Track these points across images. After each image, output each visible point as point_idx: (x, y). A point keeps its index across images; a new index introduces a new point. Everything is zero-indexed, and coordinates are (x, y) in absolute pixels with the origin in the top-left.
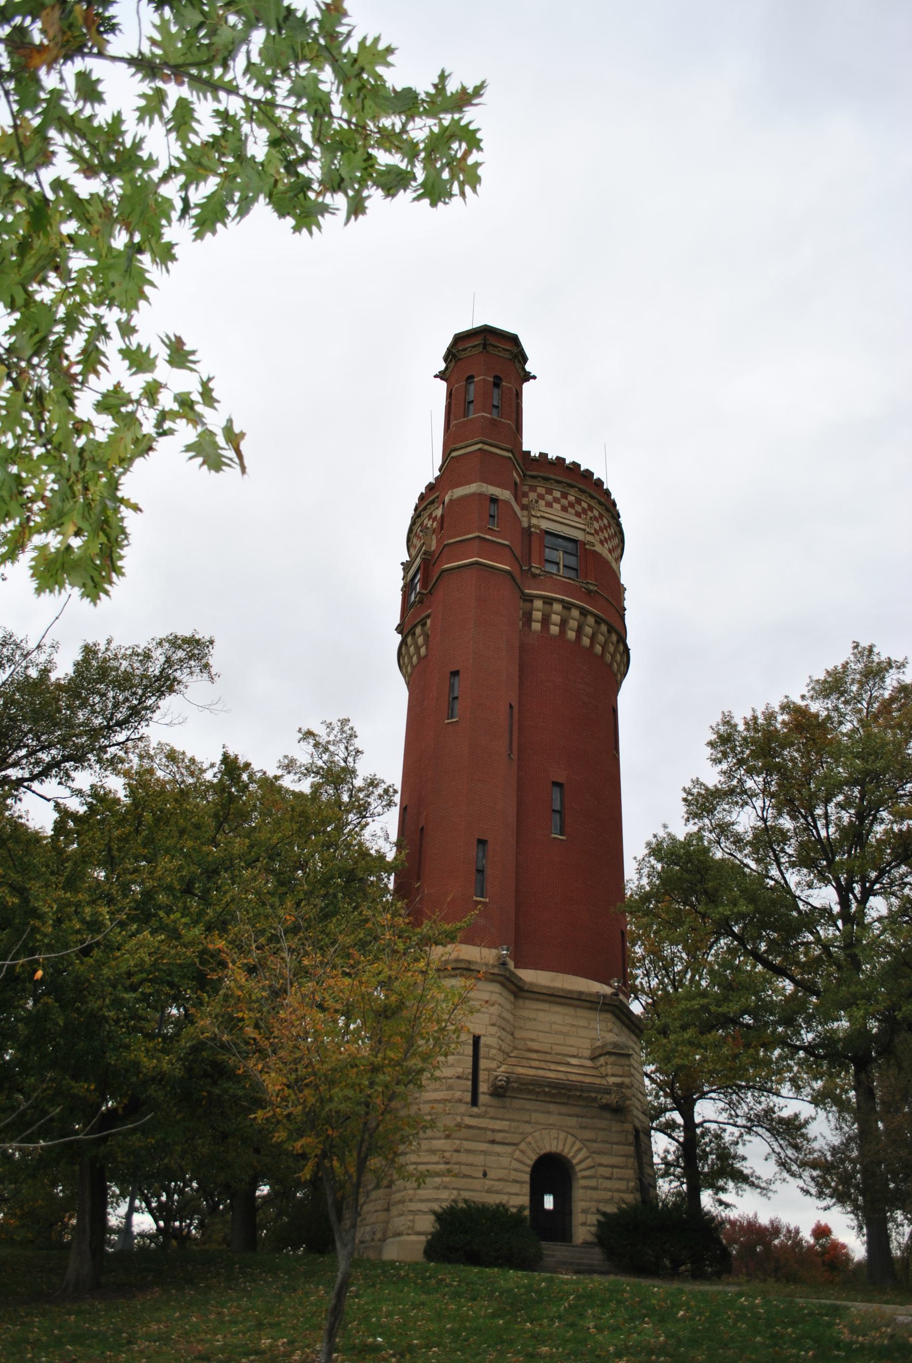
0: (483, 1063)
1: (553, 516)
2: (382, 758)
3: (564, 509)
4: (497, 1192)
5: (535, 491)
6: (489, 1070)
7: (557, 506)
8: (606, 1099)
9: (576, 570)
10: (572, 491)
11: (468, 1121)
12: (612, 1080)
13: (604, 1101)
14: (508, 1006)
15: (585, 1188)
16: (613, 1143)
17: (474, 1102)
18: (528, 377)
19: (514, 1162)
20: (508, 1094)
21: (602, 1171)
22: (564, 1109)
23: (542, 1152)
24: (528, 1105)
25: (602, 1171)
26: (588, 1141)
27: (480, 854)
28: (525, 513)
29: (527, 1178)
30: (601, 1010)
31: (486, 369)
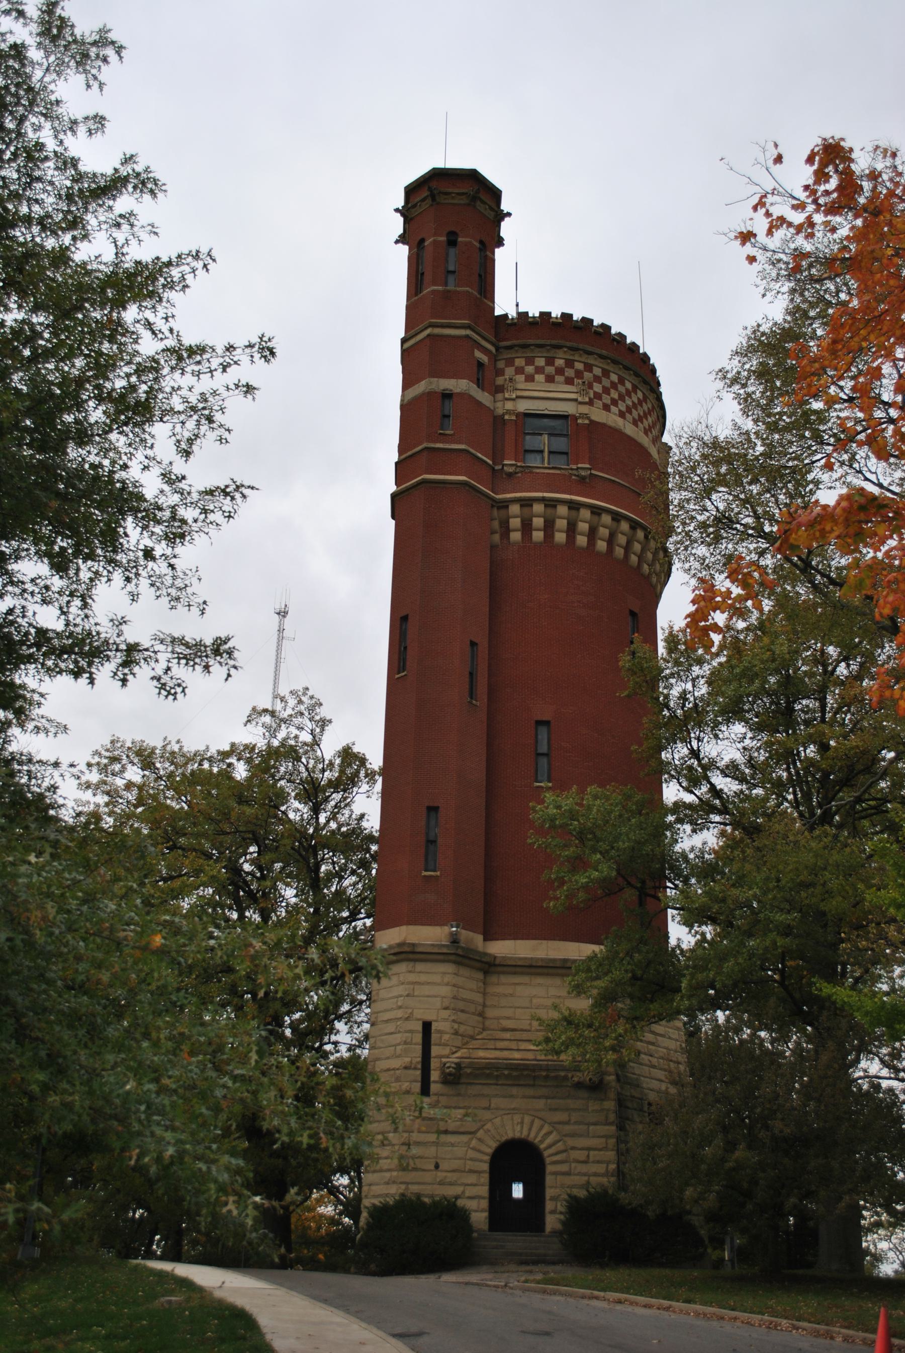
0: (435, 1051)
2: (359, 724)
7: (540, 378)
9: (566, 453)
10: (560, 353)
13: (576, 1079)
15: (556, 1173)
16: (589, 1124)
17: (425, 1090)
19: (470, 1151)
20: (462, 1081)
21: (575, 1154)
23: (504, 1139)
24: (486, 1090)
25: (575, 1154)
26: (560, 1123)
29: (486, 1167)
31: (452, 217)
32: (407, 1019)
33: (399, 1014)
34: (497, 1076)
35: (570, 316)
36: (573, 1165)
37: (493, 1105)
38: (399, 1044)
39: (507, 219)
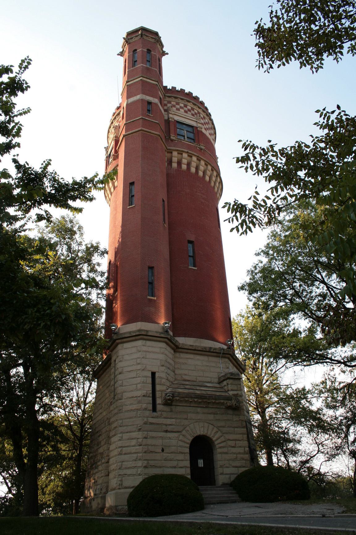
0: (158, 387)
1: (179, 114)
3: (186, 112)
4: (171, 460)
5: (170, 103)
6: (162, 391)
7: (182, 110)
8: (229, 403)
10: (189, 104)
11: (151, 420)
12: (231, 393)
13: (229, 404)
14: (171, 356)
15: (221, 453)
17: (154, 409)
18: (164, 54)
19: (179, 442)
20: (174, 404)
22: (206, 410)
23: (195, 435)
24: (188, 409)
26: (221, 427)
27: (150, 274)
28: (166, 113)
29: (187, 450)
30: (222, 357)
32: (143, 370)
33: (139, 367)
34: (191, 402)
35: (192, 94)
36: (229, 448)
37: (189, 418)
38: (139, 383)
39: (166, 56)
